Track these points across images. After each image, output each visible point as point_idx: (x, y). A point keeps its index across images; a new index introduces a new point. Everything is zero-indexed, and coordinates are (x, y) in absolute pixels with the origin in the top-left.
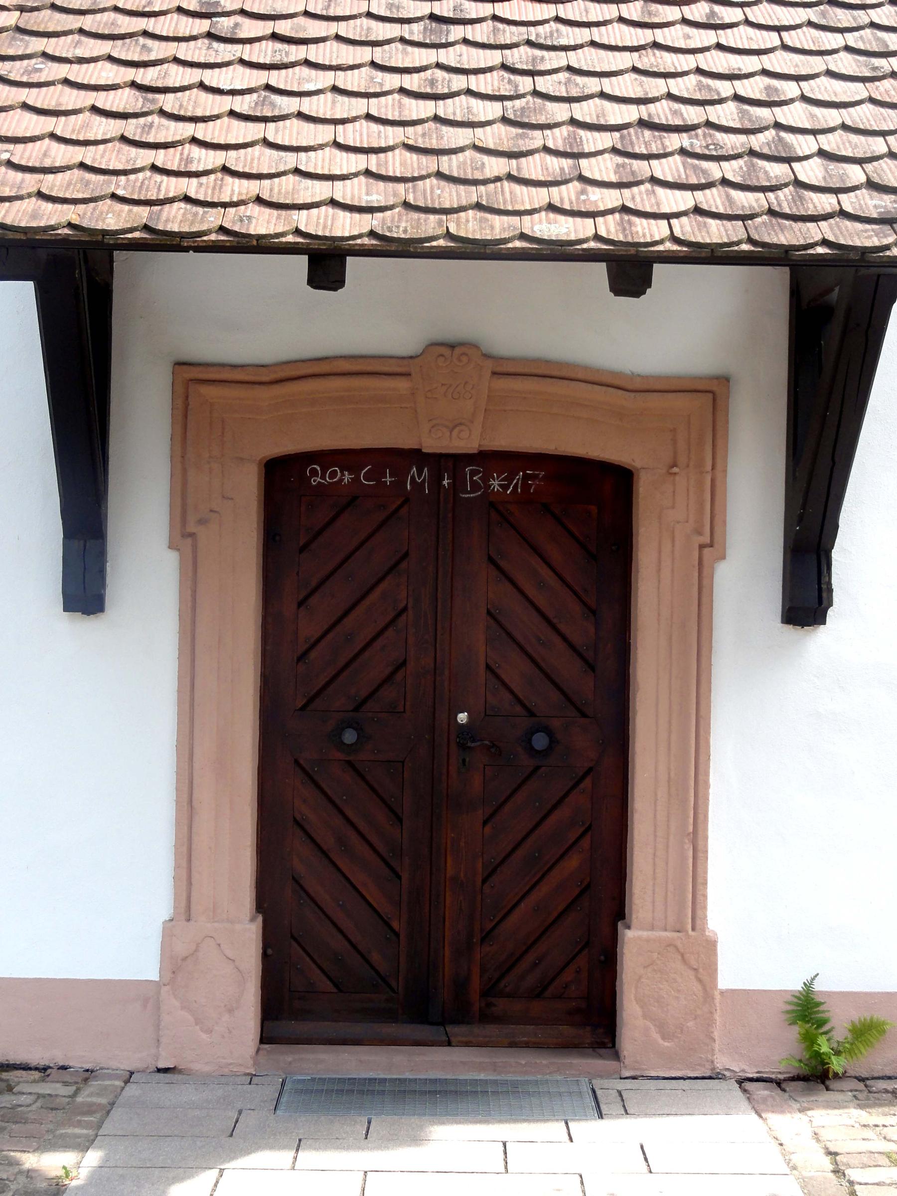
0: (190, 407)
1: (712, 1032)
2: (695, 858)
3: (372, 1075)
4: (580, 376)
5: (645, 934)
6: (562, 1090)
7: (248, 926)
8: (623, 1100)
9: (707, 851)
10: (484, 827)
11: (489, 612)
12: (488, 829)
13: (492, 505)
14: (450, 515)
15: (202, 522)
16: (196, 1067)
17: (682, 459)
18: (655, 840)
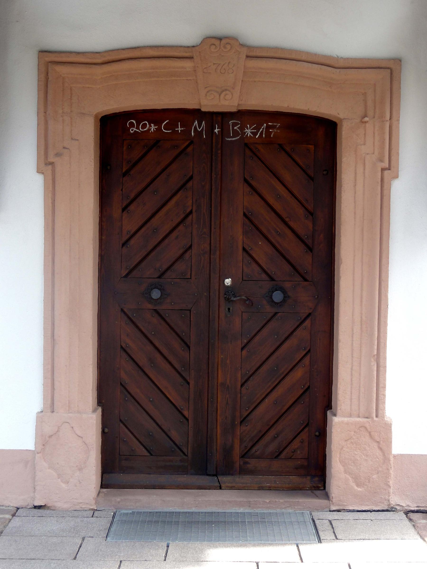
0: (49, 80)
1: (389, 482)
2: (378, 371)
3: (171, 509)
4: (304, 58)
5: (346, 419)
6: (293, 520)
7: (90, 415)
8: (333, 528)
9: (386, 367)
10: (192, 175)
11: (245, 214)
12: (244, 352)
13: (246, 145)
14: (219, 152)
15: (58, 155)
16: (59, 505)
17: (370, 113)
18: (352, 360)
